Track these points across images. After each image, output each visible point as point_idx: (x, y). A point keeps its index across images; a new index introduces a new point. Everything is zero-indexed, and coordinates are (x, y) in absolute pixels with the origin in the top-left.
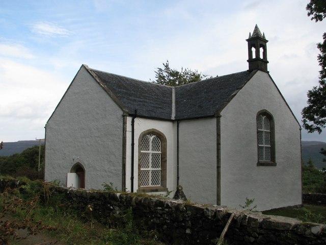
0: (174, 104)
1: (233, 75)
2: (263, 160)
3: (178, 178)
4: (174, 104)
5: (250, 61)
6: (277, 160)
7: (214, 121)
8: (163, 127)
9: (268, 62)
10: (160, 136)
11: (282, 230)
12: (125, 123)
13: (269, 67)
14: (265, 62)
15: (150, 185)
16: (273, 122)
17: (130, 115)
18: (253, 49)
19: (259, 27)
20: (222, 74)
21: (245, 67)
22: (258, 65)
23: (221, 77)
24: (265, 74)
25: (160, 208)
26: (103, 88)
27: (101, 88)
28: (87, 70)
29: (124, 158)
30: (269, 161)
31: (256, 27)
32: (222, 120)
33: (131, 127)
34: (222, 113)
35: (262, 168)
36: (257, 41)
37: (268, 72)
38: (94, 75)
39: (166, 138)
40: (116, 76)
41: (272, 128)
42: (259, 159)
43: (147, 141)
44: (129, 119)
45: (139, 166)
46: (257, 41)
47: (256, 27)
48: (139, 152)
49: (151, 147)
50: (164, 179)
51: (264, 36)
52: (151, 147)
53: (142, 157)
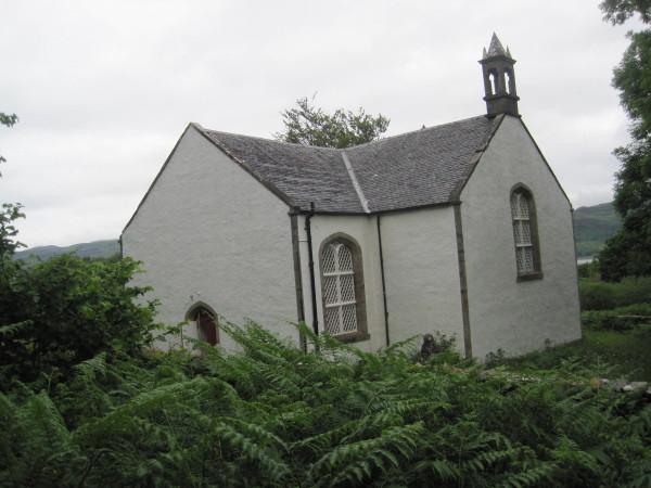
0: (356, 184)
1: (456, 125)
2: (524, 271)
3: (386, 314)
4: (356, 184)
5: (489, 99)
6: (544, 268)
7: (451, 211)
8: (355, 229)
9: (518, 99)
10: (349, 245)
11: (397, 425)
12: (294, 227)
13: (522, 108)
14: (513, 99)
15: (342, 332)
16: (534, 203)
17: (303, 213)
18: (492, 78)
19: (497, 35)
20: (433, 122)
21: (482, 109)
22: (503, 104)
23: (433, 131)
24: (516, 121)
25: (320, 384)
26: (241, 165)
27: (236, 165)
28: (202, 133)
29: (299, 290)
30: (531, 270)
31: (495, 37)
32: (464, 209)
33: (305, 233)
34: (462, 198)
35: (523, 284)
36: (497, 63)
37: (520, 117)
38: (212, 138)
39: (359, 248)
40: (243, 138)
41: (533, 214)
42: (518, 269)
43: (332, 252)
44: (301, 221)
45: (324, 300)
46: (497, 63)
47: (495, 37)
48: (322, 276)
49: (337, 265)
50: (362, 317)
51: (509, 54)
52: (337, 265)
53: (326, 280)
